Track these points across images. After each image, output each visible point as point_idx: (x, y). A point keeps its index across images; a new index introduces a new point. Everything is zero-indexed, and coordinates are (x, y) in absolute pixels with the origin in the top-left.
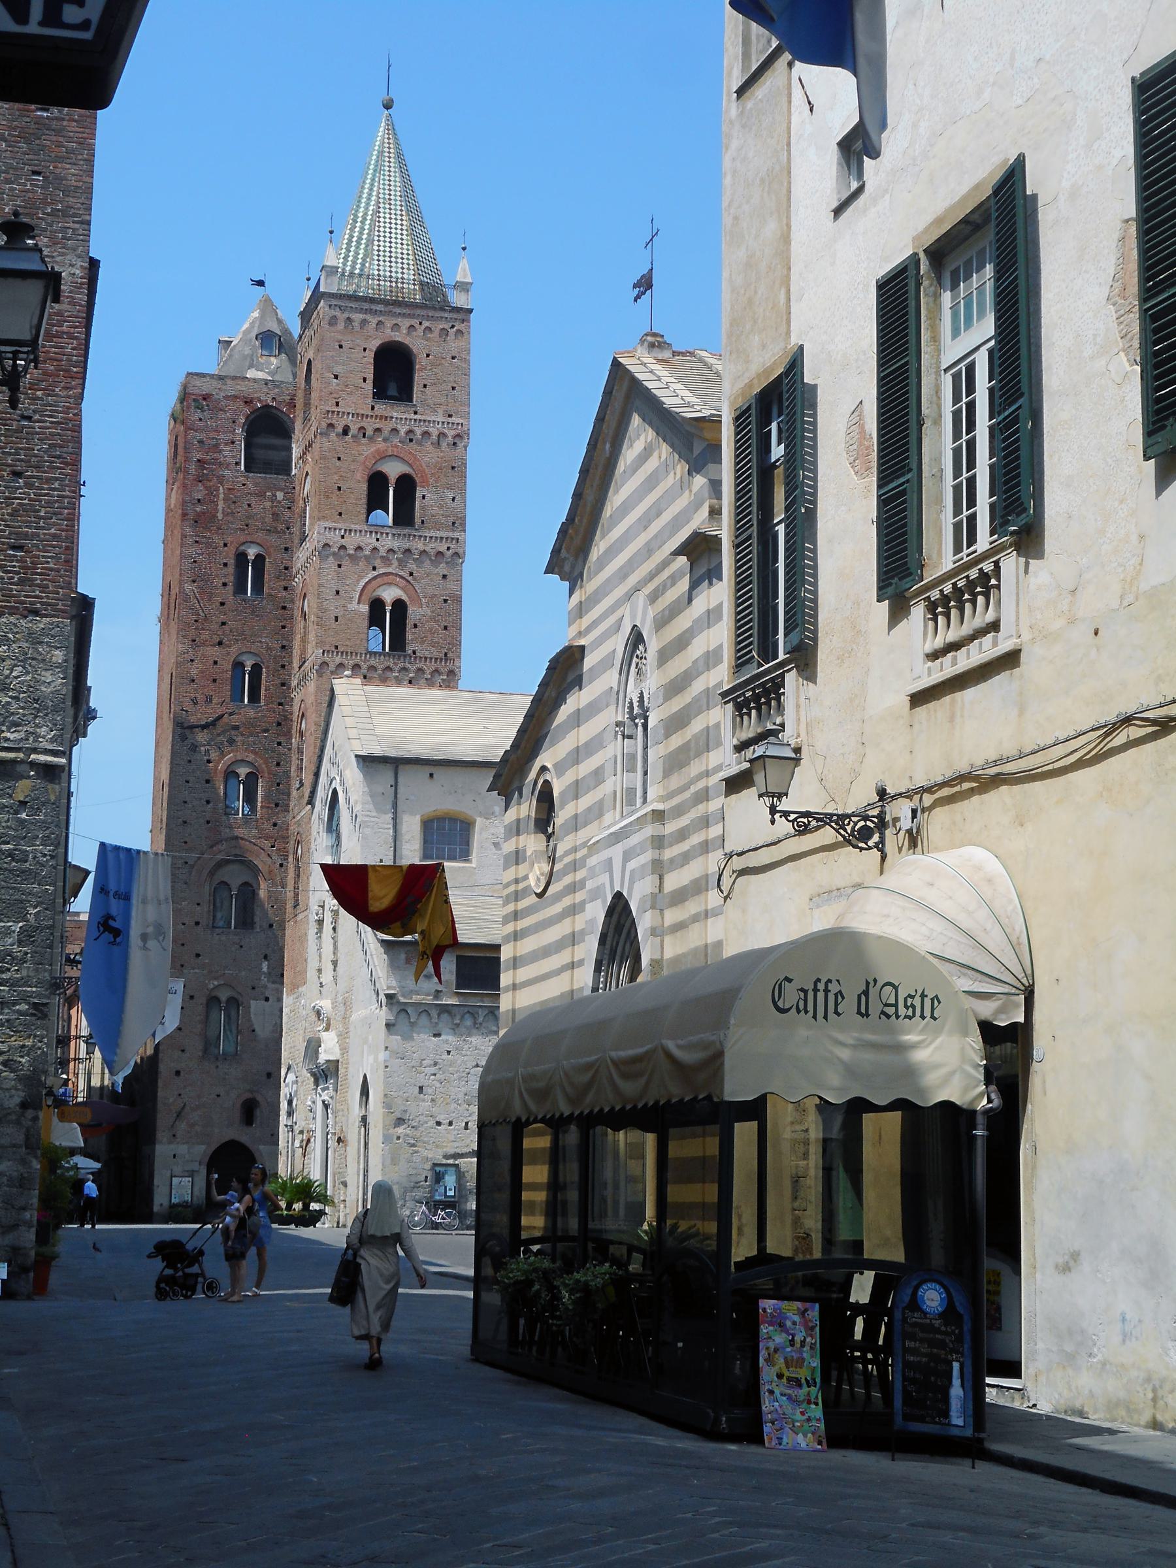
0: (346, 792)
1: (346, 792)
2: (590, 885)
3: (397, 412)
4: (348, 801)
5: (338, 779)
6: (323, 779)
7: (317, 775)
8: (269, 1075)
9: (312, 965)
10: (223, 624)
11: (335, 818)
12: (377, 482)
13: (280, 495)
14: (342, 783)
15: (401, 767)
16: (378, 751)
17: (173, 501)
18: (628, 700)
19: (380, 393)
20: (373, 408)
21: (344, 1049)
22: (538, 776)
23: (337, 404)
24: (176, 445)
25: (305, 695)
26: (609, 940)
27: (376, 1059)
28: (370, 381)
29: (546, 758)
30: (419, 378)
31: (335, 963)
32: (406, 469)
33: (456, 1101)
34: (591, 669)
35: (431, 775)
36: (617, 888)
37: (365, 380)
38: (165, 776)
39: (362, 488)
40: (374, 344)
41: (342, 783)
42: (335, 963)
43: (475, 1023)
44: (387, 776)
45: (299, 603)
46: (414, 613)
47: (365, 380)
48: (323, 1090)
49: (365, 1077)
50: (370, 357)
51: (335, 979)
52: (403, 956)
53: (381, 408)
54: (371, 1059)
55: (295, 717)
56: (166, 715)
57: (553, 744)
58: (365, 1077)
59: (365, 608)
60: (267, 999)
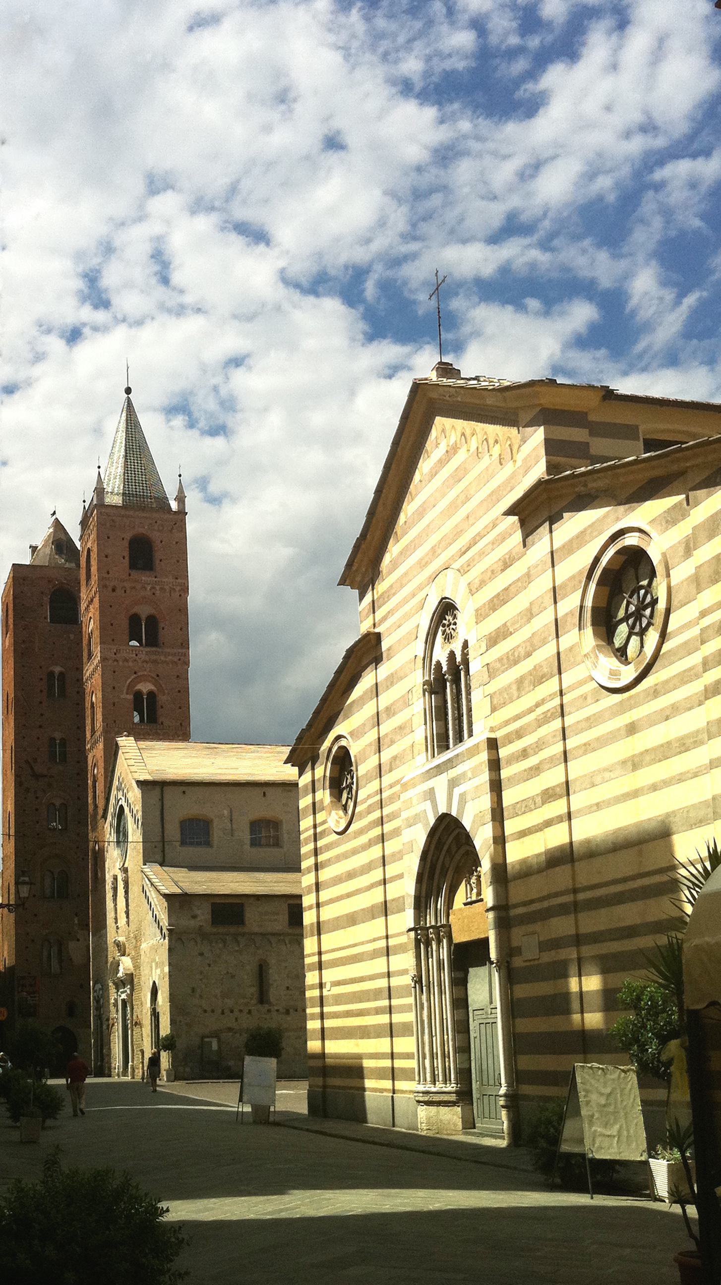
0: (129, 805)
1: (129, 805)
2: (405, 815)
3: (145, 578)
4: (131, 811)
5: (123, 799)
6: (112, 801)
7: (107, 800)
8: (81, 986)
9: (110, 915)
10: (42, 715)
11: (122, 823)
12: (134, 620)
13: (72, 636)
14: (127, 800)
15: (165, 788)
16: (149, 777)
17: (7, 644)
18: (434, 663)
19: (133, 566)
20: (130, 575)
21: (137, 967)
22: (333, 743)
23: (108, 573)
24: (7, 611)
25: (96, 753)
26: (430, 857)
27: (162, 970)
28: (127, 558)
29: (341, 728)
30: (158, 555)
31: (127, 913)
32: (153, 612)
33: (216, 996)
34: (389, 649)
35: (184, 792)
36: (442, 809)
37: (124, 558)
38: (11, 808)
39: (125, 624)
40: (128, 536)
41: (127, 800)
42: (127, 913)
43: (225, 946)
44: (157, 791)
45: (88, 698)
46: (162, 699)
47: (124, 558)
48: (122, 993)
49: (154, 982)
50: (126, 544)
51: (128, 923)
52: (177, 904)
53: (135, 574)
54: (158, 971)
55: (89, 768)
56: (9, 772)
57: (347, 717)
58: (154, 982)
59: (130, 697)
60: (78, 940)
